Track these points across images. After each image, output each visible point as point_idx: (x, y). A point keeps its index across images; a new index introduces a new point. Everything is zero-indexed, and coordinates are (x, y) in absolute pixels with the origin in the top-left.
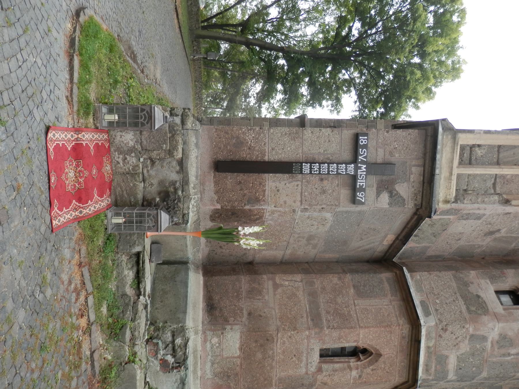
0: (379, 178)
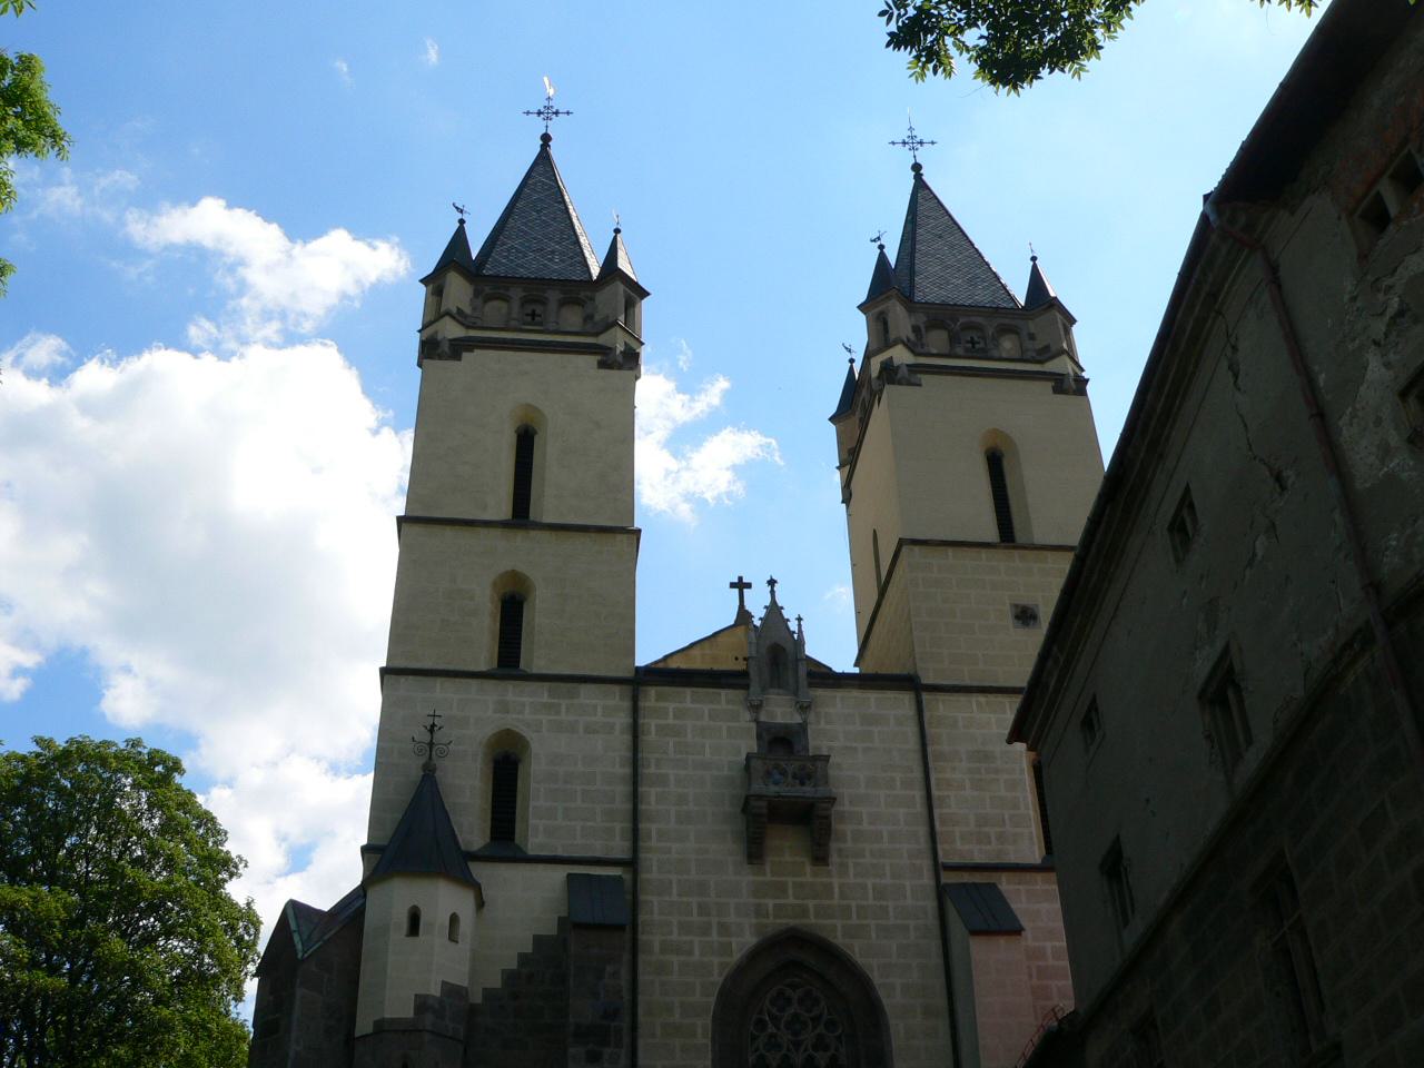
0: (599, 357)
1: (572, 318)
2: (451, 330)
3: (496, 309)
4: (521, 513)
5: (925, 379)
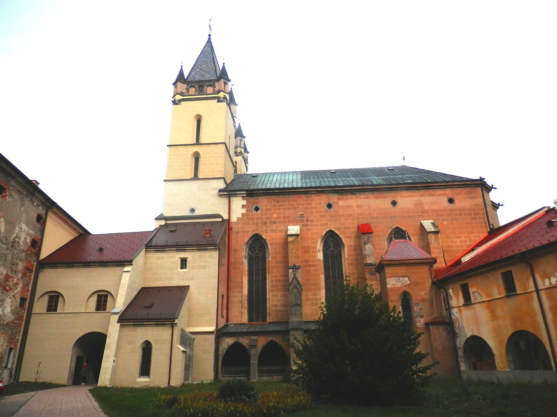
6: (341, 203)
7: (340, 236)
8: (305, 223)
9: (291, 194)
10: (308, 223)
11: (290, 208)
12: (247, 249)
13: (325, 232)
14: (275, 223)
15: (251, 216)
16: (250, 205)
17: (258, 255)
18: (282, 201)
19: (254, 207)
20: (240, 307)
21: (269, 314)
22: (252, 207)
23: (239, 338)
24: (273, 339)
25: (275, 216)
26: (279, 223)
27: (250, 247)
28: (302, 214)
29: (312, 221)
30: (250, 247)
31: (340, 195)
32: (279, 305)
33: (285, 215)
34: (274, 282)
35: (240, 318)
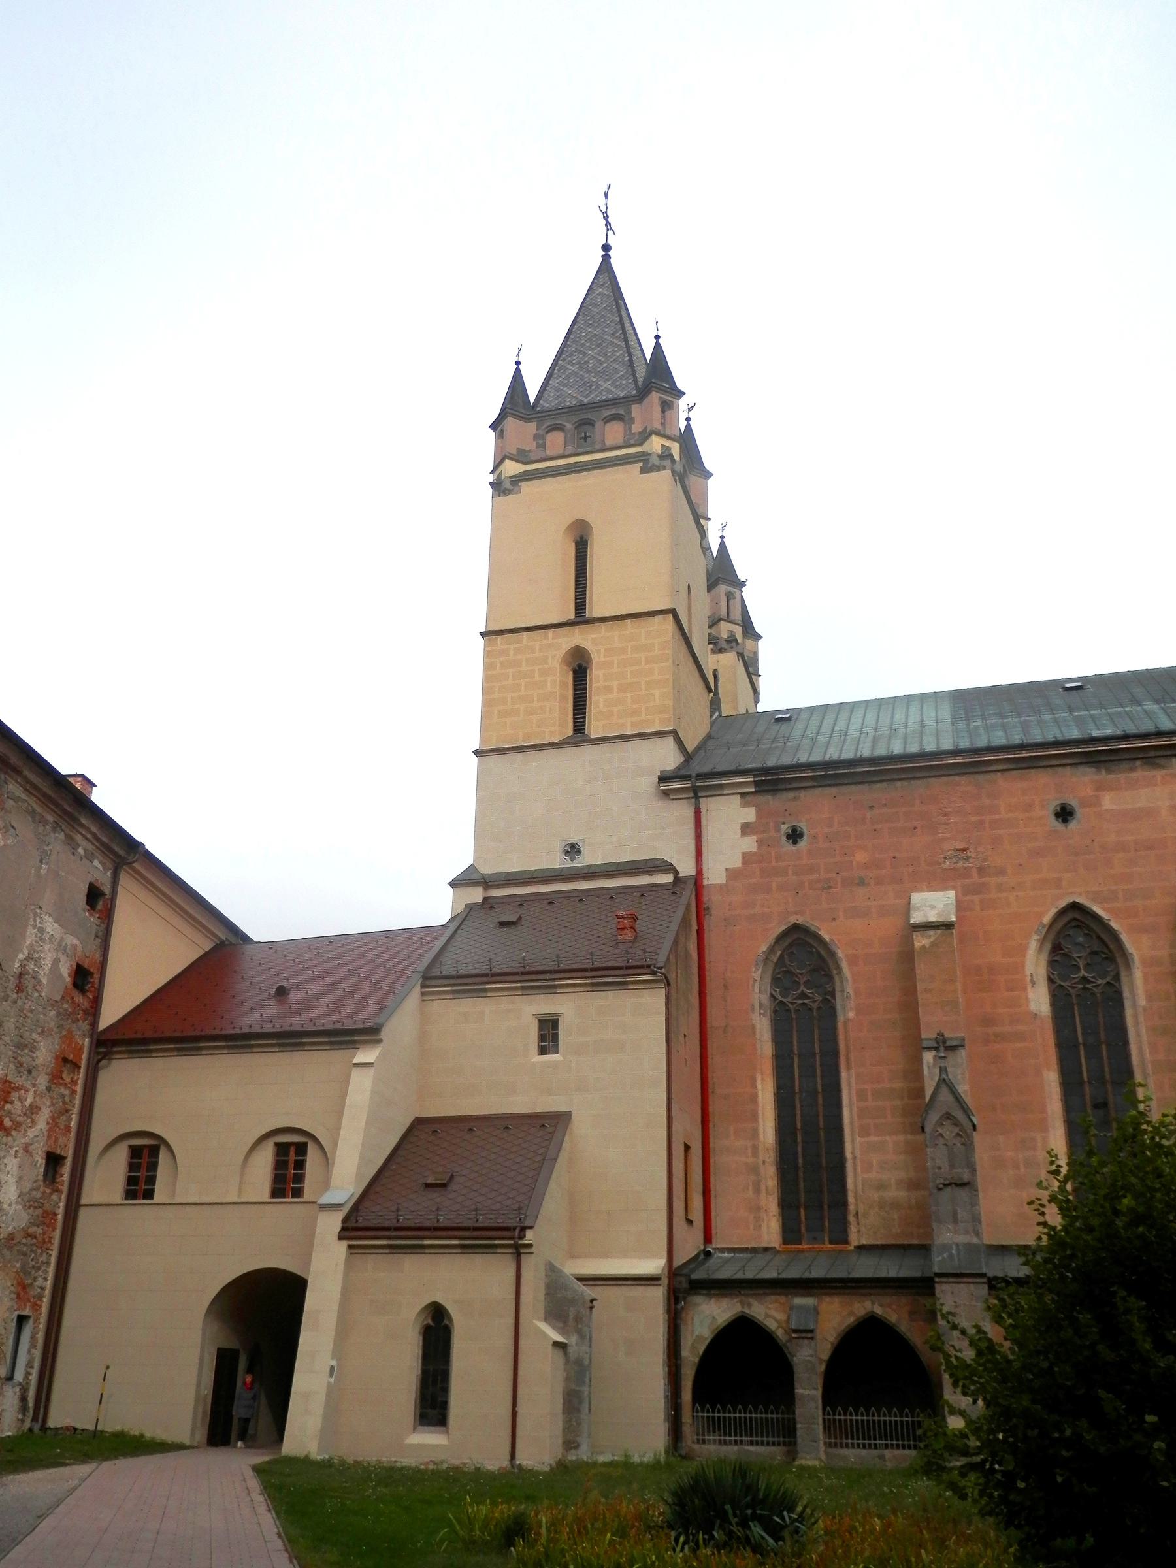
1: (614, 432)
2: (512, 468)
3: (556, 441)
4: (581, 617)
5: (524, 486)
6: (1108, 802)
7: (1114, 925)
8: (976, 878)
9: (918, 775)
10: (987, 879)
11: (915, 828)
12: (768, 980)
13: (1053, 911)
14: (861, 882)
15: (774, 864)
16: (772, 824)
17: (806, 1001)
18: (885, 805)
19: (784, 828)
20: (751, 1188)
21: (857, 1214)
22: (779, 830)
23: (751, 1300)
24: (875, 1310)
25: (861, 857)
26: (879, 882)
27: (777, 971)
28: (962, 846)
29: (1001, 872)
30: (779, 973)
31: (1103, 771)
32: (893, 1181)
33: (896, 855)
34: (870, 1098)
35: (752, 1227)
